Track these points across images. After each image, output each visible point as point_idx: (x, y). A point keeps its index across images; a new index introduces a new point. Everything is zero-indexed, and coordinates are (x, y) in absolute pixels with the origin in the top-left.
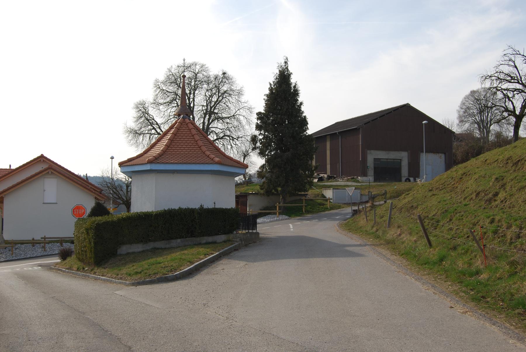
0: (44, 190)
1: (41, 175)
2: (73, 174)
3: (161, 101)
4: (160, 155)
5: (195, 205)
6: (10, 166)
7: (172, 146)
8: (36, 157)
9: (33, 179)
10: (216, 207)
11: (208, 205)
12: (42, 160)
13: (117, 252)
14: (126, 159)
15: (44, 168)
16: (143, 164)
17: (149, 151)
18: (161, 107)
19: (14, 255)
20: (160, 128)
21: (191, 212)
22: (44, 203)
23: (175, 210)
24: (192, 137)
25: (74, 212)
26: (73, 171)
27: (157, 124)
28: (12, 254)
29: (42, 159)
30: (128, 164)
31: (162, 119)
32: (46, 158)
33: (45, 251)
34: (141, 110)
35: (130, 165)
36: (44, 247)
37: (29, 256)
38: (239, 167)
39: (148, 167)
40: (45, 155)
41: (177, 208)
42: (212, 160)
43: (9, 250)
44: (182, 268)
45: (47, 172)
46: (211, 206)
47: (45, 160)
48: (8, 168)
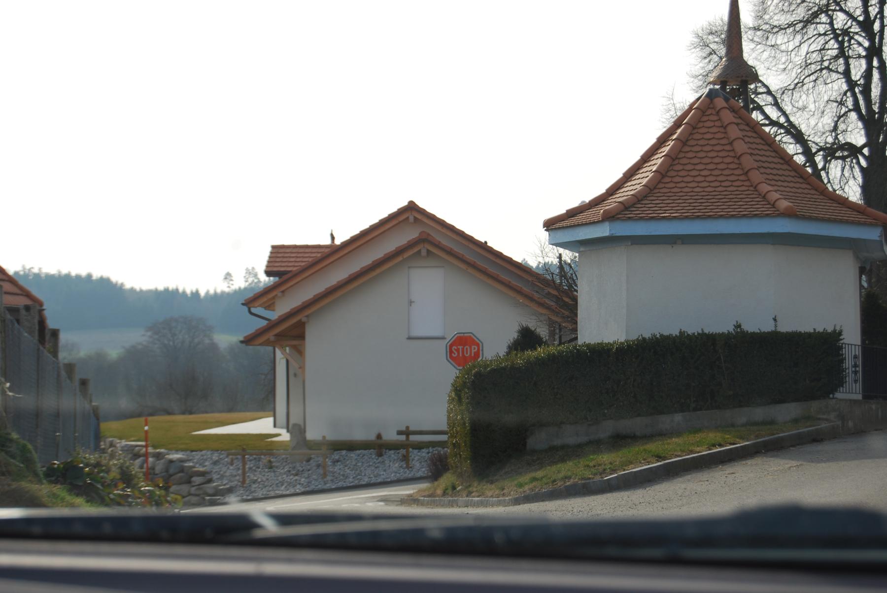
0: (411, 302)
1: (400, 259)
2: (509, 260)
3: (782, 19)
4: (639, 199)
5: (721, 325)
6: (333, 238)
7: (679, 167)
8: (393, 209)
9: (378, 271)
10: (859, 343)
11: (757, 323)
12: (411, 219)
13: (525, 445)
14: (563, 211)
15: (415, 238)
16: (594, 223)
17: (619, 188)
18: (780, 39)
19: (329, 478)
20: (776, 104)
21: (707, 341)
22: (409, 338)
23: (668, 338)
24: (728, 148)
25: (451, 352)
26: (506, 253)
27: (769, 92)
28: (325, 475)
29: (411, 213)
30: (564, 224)
31: (783, 76)
32: (423, 212)
33: (408, 467)
34: (714, 52)
35: (567, 227)
36: (406, 458)
37: (366, 480)
38: (864, 224)
39: (603, 231)
40: (421, 204)
41: (675, 332)
42: (773, 205)
43: (318, 466)
44: (631, 466)
45: (415, 250)
46: (767, 327)
47: (419, 216)
48: (327, 241)
